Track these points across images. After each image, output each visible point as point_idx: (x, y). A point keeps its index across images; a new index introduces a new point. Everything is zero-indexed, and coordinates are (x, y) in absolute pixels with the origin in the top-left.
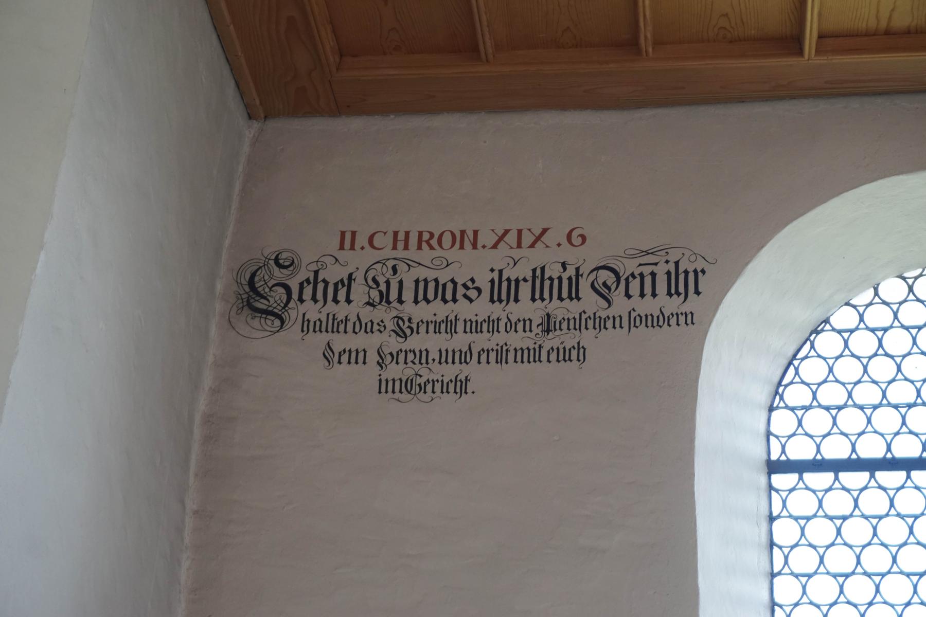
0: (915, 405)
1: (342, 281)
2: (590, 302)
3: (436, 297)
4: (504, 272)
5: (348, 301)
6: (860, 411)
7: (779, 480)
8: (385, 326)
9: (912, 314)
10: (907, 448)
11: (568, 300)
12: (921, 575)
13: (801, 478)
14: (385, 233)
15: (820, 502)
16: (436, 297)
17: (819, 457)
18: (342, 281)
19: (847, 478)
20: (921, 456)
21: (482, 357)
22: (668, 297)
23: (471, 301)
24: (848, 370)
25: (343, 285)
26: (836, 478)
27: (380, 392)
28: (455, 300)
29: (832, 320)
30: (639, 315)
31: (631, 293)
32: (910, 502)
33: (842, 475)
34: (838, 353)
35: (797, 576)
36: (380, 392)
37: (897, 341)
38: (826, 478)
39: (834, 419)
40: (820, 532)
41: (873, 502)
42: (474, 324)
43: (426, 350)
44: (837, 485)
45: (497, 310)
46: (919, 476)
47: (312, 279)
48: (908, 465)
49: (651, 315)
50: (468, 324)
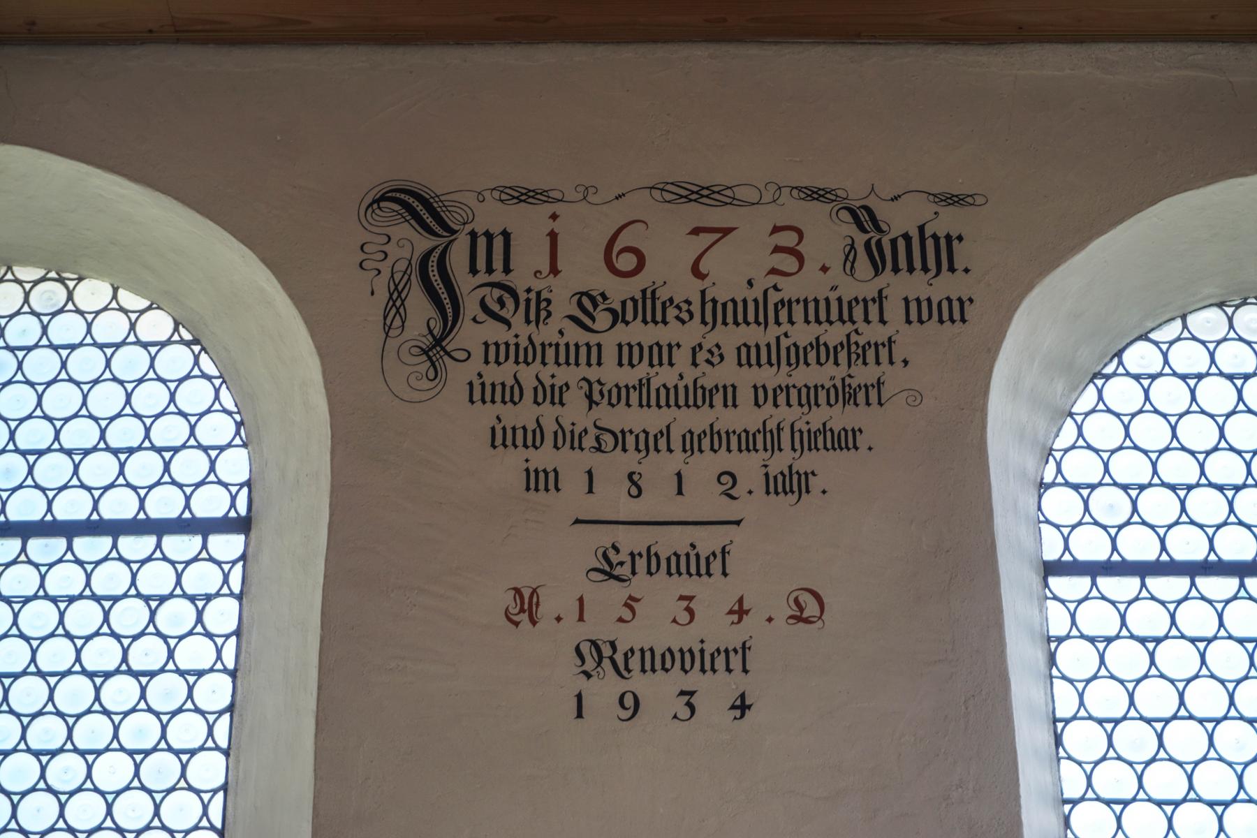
0: (1245, 486)
5: (883, 321)
6: (1121, 492)
7: (1059, 584)
8: (722, 357)
9: (1234, 357)
10: (1236, 545)
13: (1094, 583)
16: (635, 318)
19: (1158, 585)
20: (1158, 559)
21: (715, 398)
23: (683, 322)
24: (1151, 432)
26: (1094, 583)
28: (665, 322)
30: (795, 345)
32: (1243, 619)
33: (1201, 581)
34: (1231, 408)
35: (1149, 721)
37: (1217, 395)
38: (1130, 585)
39: (1183, 503)
40: (1127, 658)
41: (1147, 618)
42: (753, 351)
44: (1144, 594)
46: (1256, 585)
48: (1241, 570)
49: (639, 344)
50: (492, 349)
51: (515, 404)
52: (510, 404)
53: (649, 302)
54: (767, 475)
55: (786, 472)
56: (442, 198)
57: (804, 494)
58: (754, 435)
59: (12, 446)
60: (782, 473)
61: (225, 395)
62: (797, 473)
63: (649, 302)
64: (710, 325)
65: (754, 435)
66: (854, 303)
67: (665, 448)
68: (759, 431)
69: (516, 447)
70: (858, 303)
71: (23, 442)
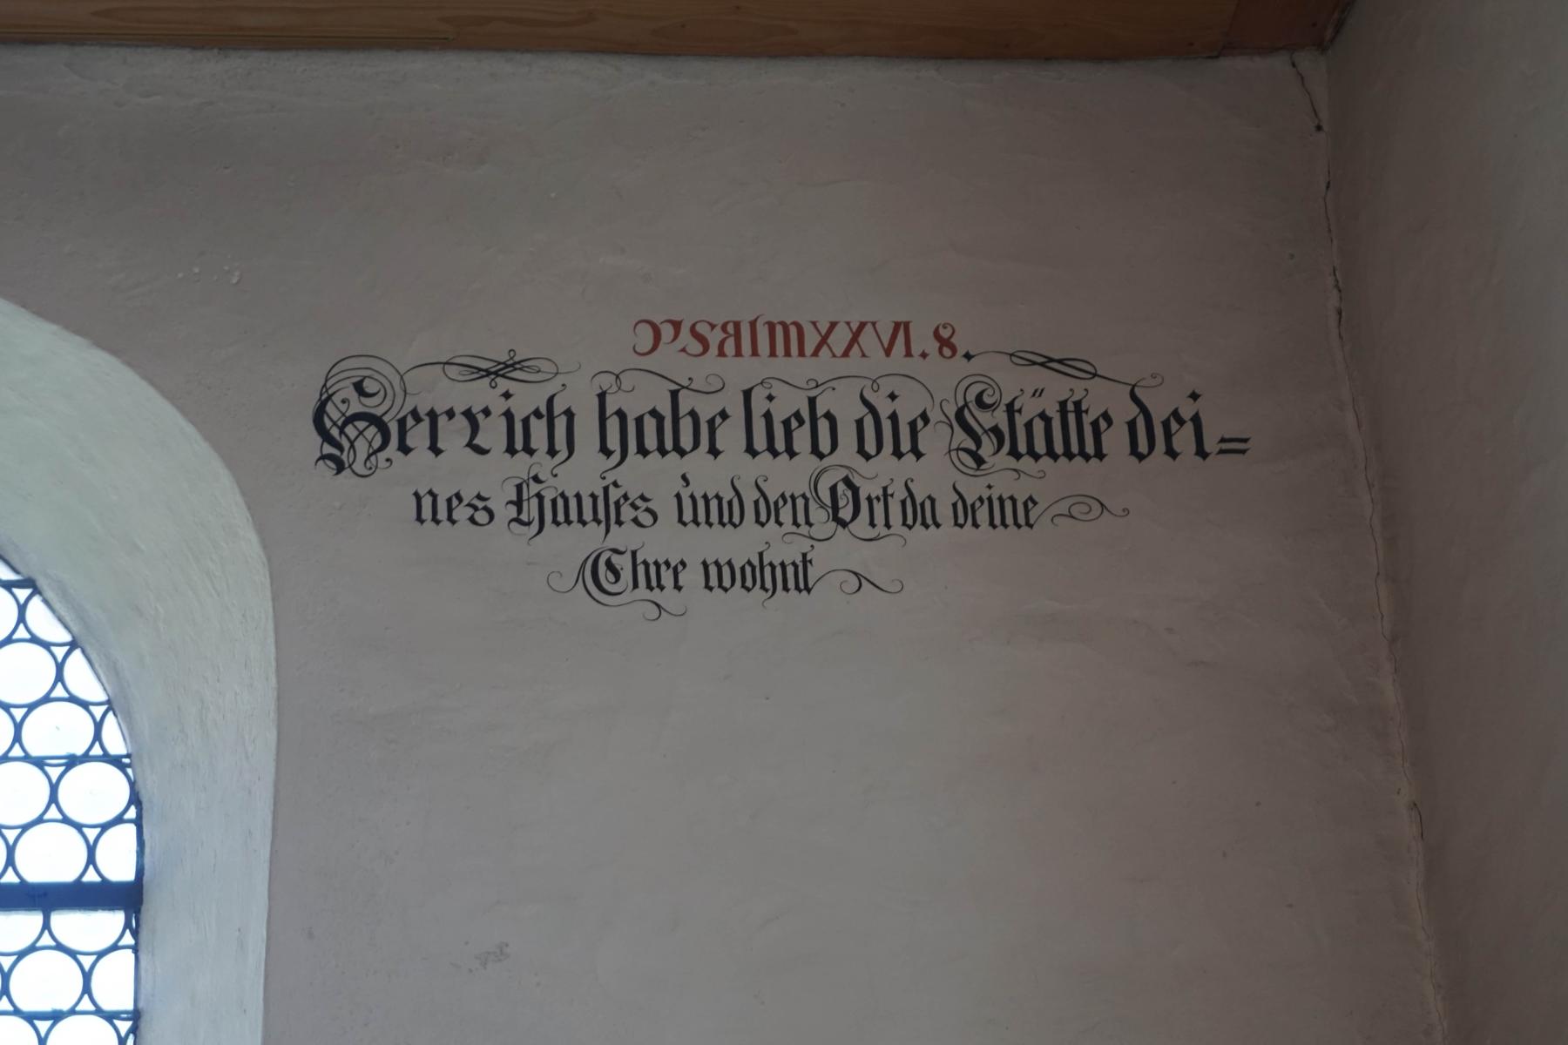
1: (797, 415)
2: (935, 473)
3: (696, 445)
4: (609, 399)
11: (768, 455)
12: (5, 759)
14: (683, 350)
15: (91, 850)
16: (696, 445)
17: (91, 877)
18: (797, 415)
22: (711, 457)
25: (801, 422)
27: (420, 519)
29: (36, 600)
31: (533, 445)
36: (420, 519)
43: (430, 492)
45: (749, 471)
47: (806, 415)
51: (735, 526)
52: (729, 527)
53: (1072, 418)
54: (1222, 452)
55: (756, 562)
56: (954, 446)
57: (614, 527)
58: (526, 422)
59: (17, 753)
60: (749, 562)
61: (77, 668)
62: (771, 564)
63: (1072, 418)
64: (616, 457)
65: (526, 422)
66: (410, 422)
67: (791, 520)
68: (537, 414)
69: (1006, 526)
70: (418, 420)
71: (36, 741)
